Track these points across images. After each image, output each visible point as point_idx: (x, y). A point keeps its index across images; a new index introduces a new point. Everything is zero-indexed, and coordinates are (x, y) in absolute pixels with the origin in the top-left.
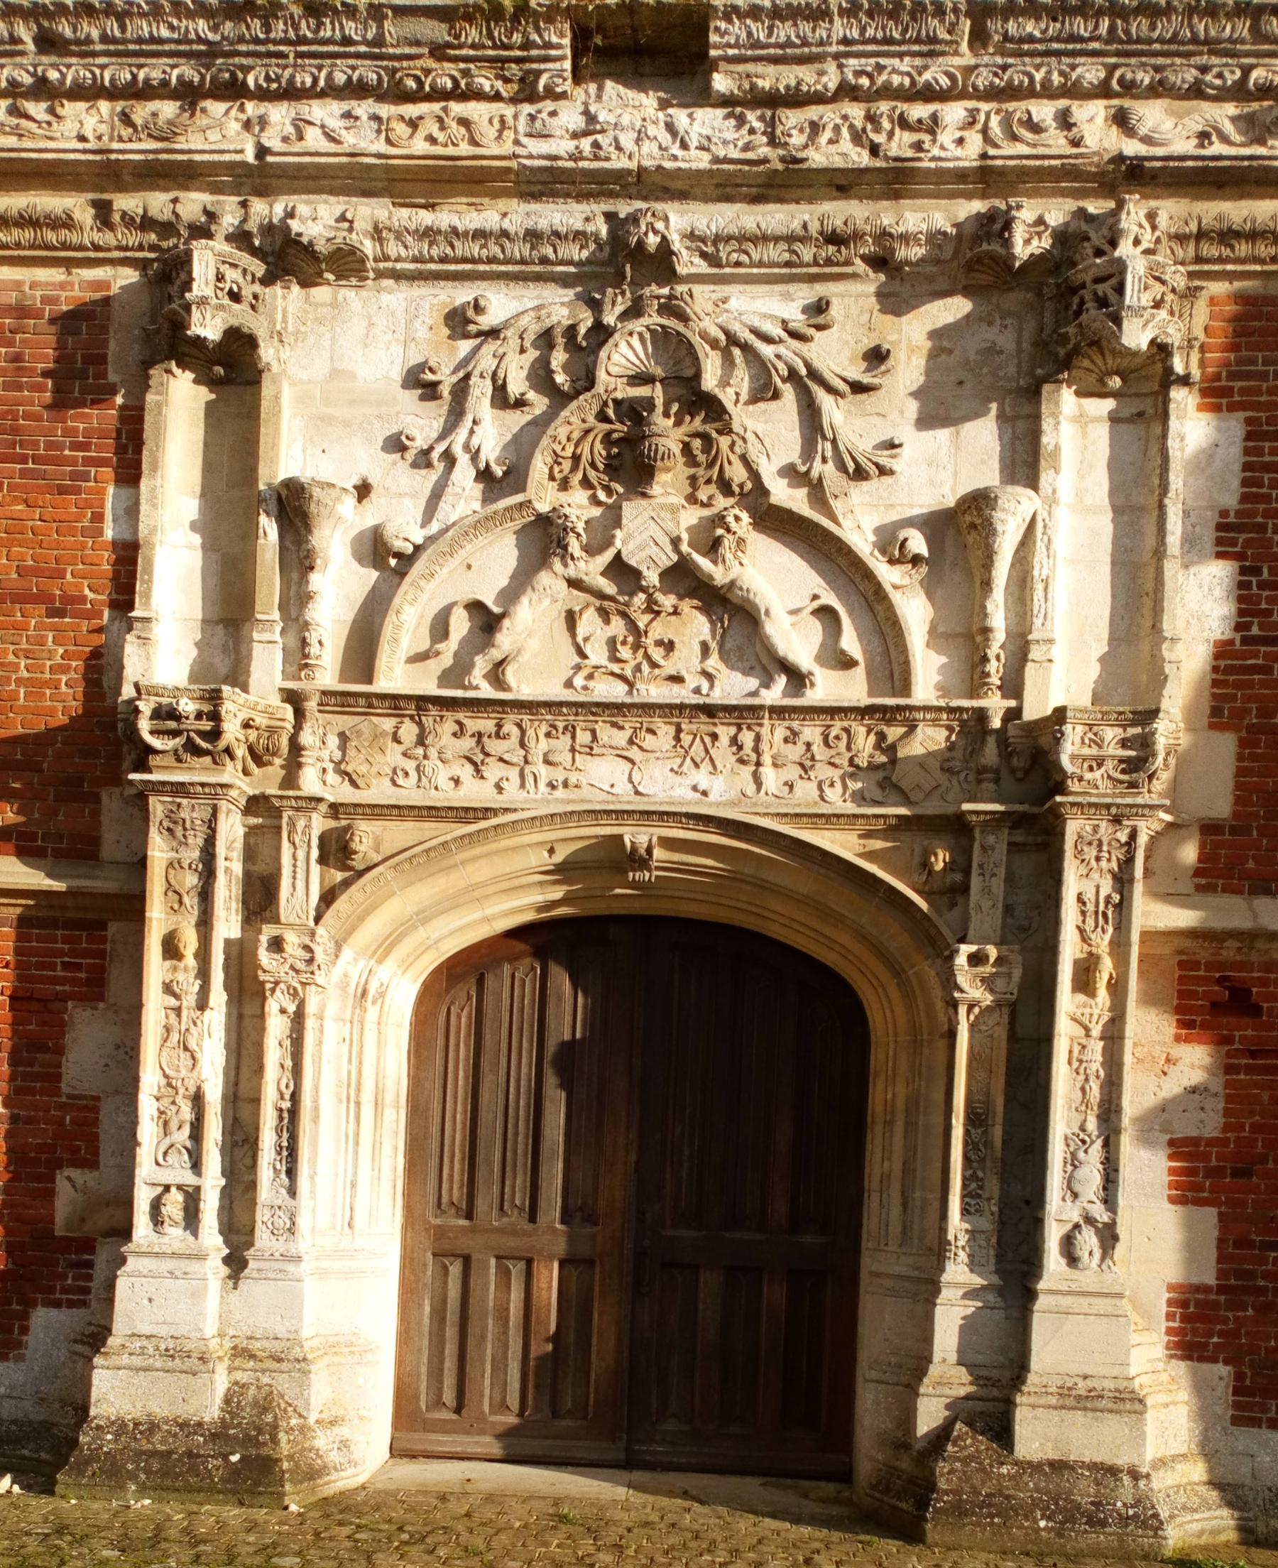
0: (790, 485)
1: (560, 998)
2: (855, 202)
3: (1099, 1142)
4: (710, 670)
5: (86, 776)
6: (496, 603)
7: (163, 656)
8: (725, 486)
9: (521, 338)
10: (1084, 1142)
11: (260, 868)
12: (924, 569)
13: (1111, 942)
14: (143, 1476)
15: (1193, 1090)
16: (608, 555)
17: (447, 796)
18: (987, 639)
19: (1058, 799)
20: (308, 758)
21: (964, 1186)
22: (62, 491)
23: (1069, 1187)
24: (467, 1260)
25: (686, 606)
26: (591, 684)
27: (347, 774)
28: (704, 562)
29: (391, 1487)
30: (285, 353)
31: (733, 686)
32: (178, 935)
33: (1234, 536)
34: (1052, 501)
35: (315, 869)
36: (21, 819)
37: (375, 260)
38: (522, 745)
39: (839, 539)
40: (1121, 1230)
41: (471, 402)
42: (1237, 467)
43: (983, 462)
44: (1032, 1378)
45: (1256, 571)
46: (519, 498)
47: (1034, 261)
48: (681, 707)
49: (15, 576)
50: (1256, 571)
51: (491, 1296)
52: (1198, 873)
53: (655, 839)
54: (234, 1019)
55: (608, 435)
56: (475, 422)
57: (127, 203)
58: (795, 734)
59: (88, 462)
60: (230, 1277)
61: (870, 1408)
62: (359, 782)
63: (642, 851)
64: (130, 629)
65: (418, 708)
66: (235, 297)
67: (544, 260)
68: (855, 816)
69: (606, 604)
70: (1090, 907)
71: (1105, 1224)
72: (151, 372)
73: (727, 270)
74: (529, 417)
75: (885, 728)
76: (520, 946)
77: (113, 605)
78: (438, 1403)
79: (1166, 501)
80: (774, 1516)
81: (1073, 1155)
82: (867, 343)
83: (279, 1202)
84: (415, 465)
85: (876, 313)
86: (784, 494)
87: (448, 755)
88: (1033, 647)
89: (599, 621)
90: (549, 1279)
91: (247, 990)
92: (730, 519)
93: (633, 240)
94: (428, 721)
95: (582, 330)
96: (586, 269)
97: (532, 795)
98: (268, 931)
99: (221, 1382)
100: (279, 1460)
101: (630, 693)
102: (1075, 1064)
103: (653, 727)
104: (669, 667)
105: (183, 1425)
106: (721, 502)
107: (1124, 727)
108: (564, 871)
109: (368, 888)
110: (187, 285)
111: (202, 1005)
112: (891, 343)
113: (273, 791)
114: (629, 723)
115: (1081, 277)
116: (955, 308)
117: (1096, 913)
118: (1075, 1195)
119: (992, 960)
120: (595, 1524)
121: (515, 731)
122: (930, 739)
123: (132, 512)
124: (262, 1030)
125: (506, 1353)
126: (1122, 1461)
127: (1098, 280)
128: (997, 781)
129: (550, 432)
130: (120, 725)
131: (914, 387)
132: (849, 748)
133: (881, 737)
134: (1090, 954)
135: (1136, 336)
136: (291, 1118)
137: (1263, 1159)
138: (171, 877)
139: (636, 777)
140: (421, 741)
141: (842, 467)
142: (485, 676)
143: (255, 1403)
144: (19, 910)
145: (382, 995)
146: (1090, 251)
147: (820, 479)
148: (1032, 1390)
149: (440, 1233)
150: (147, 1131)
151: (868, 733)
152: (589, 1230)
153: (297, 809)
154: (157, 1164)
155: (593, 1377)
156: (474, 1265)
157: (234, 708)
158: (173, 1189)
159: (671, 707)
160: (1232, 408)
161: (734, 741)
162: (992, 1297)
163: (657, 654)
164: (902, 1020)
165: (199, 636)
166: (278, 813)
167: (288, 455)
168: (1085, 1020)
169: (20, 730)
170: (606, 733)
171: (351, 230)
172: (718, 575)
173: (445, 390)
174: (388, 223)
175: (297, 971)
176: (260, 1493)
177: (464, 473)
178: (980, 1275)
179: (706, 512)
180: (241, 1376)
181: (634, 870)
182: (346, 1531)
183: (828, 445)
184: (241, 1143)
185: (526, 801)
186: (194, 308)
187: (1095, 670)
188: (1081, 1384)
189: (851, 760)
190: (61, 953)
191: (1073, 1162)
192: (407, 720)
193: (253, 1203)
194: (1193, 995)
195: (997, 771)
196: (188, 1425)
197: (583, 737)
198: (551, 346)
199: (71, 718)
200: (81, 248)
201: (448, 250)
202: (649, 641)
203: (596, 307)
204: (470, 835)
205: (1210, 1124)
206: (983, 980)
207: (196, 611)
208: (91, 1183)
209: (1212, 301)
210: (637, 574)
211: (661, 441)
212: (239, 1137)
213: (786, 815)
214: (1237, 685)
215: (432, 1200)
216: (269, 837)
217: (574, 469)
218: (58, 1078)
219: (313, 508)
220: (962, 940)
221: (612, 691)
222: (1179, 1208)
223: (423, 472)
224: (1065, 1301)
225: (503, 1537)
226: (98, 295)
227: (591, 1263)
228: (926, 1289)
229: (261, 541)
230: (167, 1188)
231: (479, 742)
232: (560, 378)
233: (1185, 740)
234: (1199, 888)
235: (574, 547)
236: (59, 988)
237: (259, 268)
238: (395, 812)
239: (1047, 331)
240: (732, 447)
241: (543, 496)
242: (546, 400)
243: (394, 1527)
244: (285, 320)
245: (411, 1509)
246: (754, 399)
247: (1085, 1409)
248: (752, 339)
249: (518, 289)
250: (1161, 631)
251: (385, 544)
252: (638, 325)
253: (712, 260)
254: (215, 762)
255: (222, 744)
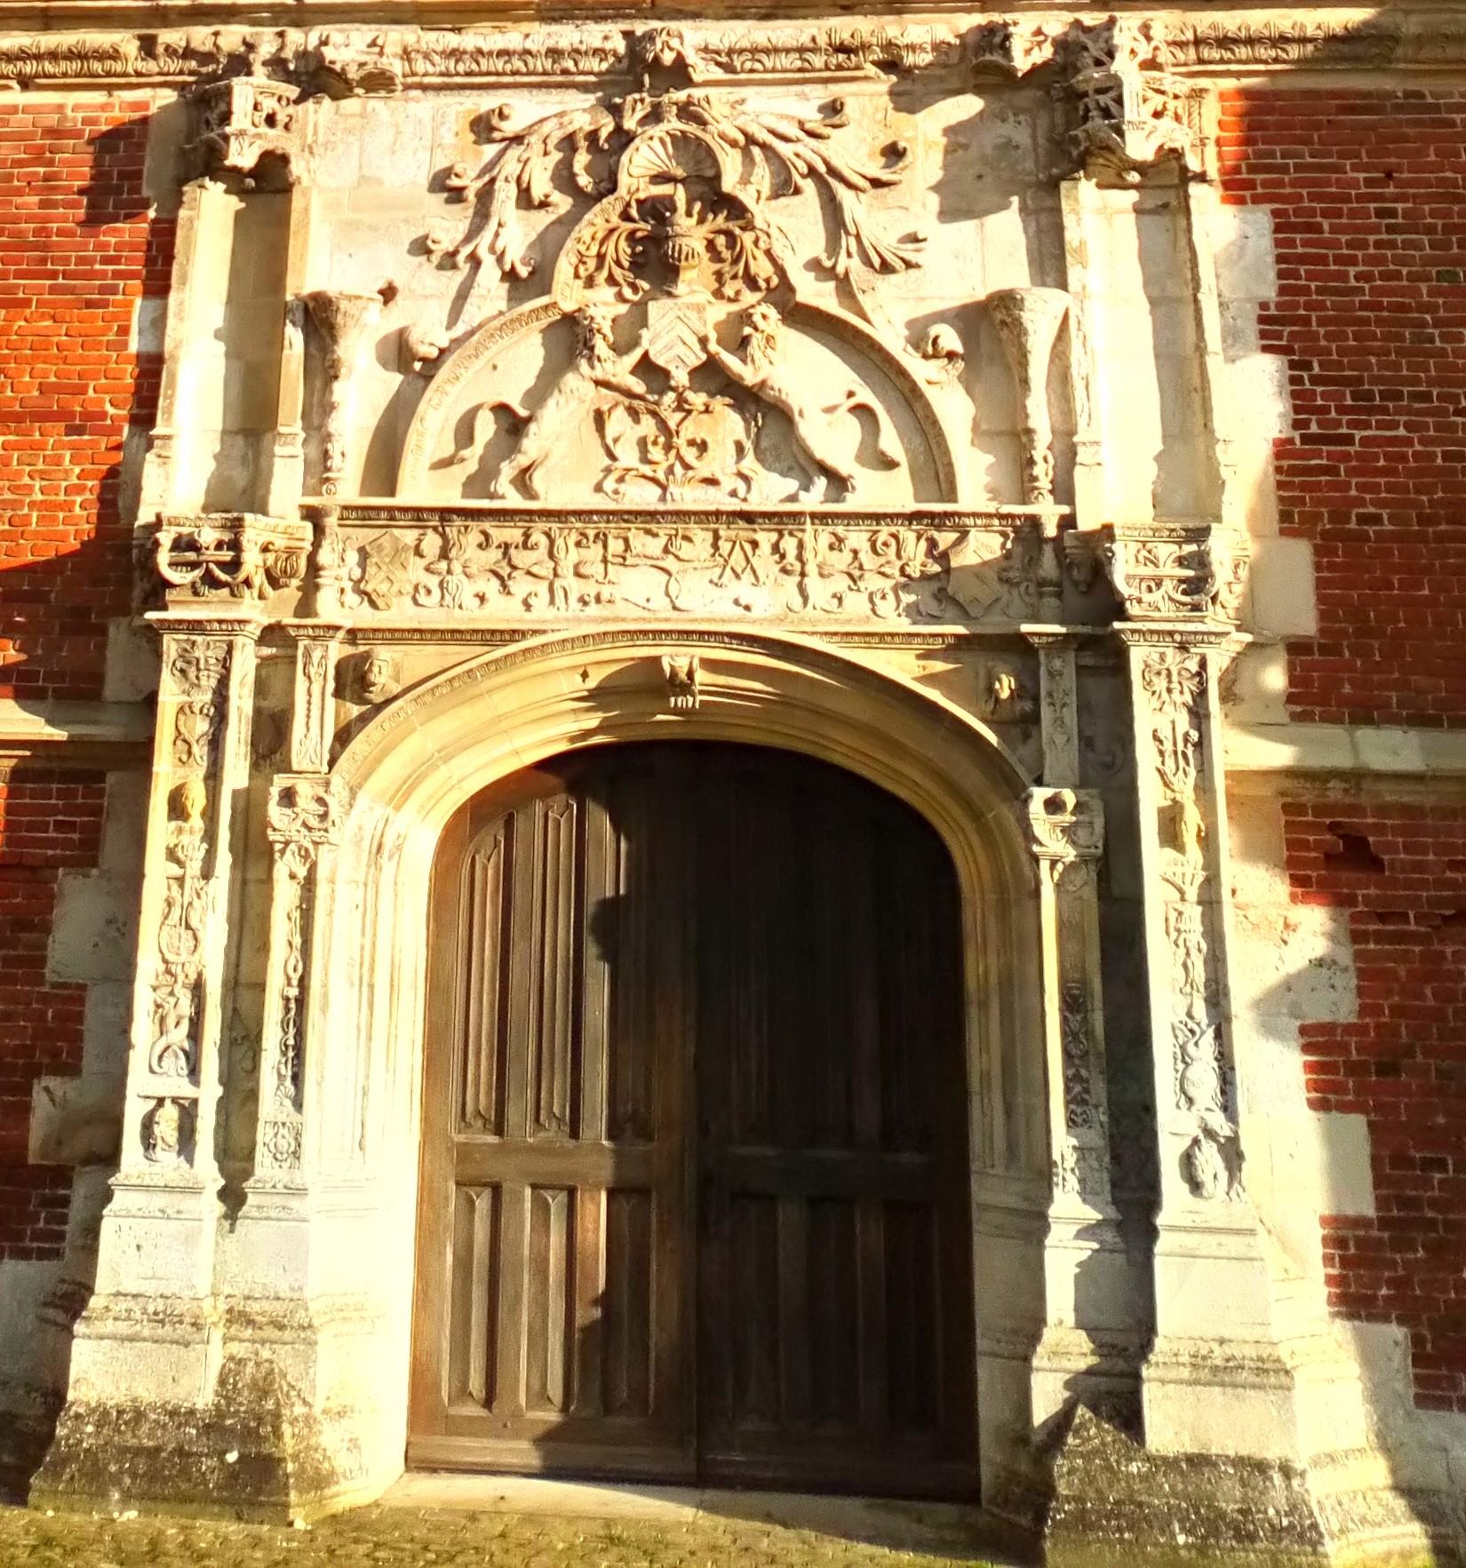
0: (817, 279)
1: (600, 843)
2: (859, 18)
3: (1210, 1033)
4: (746, 472)
5: (92, 607)
6: (523, 404)
7: (175, 488)
8: (752, 283)
9: (545, 142)
10: (1192, 1031)
11: (271, 704)
12: (960, 365)
13: (1196, 788)
14: (128, 1481)
15: (1320, 963)
16: (636, 355)
17: (471, 617)
18: (1032, 440)
19: (1117, 625)
20: (325, 579)
21: (1068, 1090)
22: (90, 304)
23: (1183, 1091)
24: (496, 1190)
25: (719, 403)
26: (622, 488)
27: (366, 594)
28: (731, 361)
29: (408, 1504)
30: (314, 164)
31: (771, 490)
32: (186, 792)
33: (1278, 329)
34: (1082, 297)
35: (331, 702)
36: (23, 657)
37: (404, 76)
38: (551, 555)
39: (868, 337)
40: (1244, 1146)
41: (496, 206)
42: (1270, 259)
43: (1010, 254)
44: (1159, 1343)
45: (1307, 366)
46: (544, 300)
47: (1035, 70)
48: (718, 514)
49: (36, 393)
50: (1307, 366)
51: (527, 1240)
52: (1291, 699)
53: (696, 663)
54: (238, 886)
55: (632, 233)
56: (500, 225)
57: (170, 37)
58: (841, 540)
59: (118, 275)
60: (226, 1217)
61: (990, 1409)
62: (380, 602)
63: (683, 676)
64: (150, 446)
65: (442, 520)
66: (271, 120)
67: (565, 72)
68: (910, 635)
69: (636, 403)
70: (1168, 746)
71: (1227, 1138)
72: (185, 188)
73: (743, 76)
74: (553, 217)
75: (936, 535)
76: (552, 780)
77: (134, 420)
78: (463, 1393)
79: (1200, 296)
80: (870, 1540)
81: (1183, 1048)
82: (884, 140)
83: (281, 1118)
84: (440, 267)
85: (890, 111)
86: (814, 293)
87: (473, 570)
88: (1080, 449)
89: (628, 420)
90: (596, 1213)
91: (254, 851)
92: (757, 318)
93: (650, 57)
94: (451, 532)
95: (604, 134)
96: (607, 78)
97: (563, 613)
98: (280, 781)
99: (215, 1355)
100: (282, 1460)
101: (663, 499)
102: (1174, 935)
103: (689, 534)
104: (703, 469)
105: (173, 1413)
106: (749, 297)
107: (1179, 544)
108: (599, 697)
109: (386, 726)
110: (226, 118)
111: (207, 874)
112: (907, 140)
113: (289, 620)
114: (664, 530)
115: (1082, 87)
116: (968, 106)
117: (1175, 753)
118: (1190, 1101)
119: (1070, 806)
120: (652, 1545)
121: (544, 541)
122: (983, 547)
123: (158, 324)
124: (268, 898)
125: (545, 1322)
126: (1272, 1454)
127: (1100, 91)
128: (1059, 595)
129: (574, 235)
130: (135, 551)
131: (933, 182)
132: (899, 556)
133: (932, 544)
134: (1174, 800)
135: (1140, 147)
136: (298, 1007)
137: (1409, 1052)
138: (181, 723)
139: (673, 591)
140: (444, 554)
141: (868, 262)
142: (512, 482)
143: (254, 1385)
144: (13, 762)
145: (399, 848)
146: (1090, 61)
147: (847, 274)
148: (1161, 1360)
149: (464, 1154)
150: (142, 1030)
151: (919, 538)
152: (641, 1147)
153: (314, 638)
154: (152, 1071)
155: (653, 1355)
156: (505, 1198)
157: (255, 530)
158: (168, 1103)
159: (707, 514)
160: (1257, 200)
161: (776, 548)
162: (1110, 1236)
163: (690, 454)
164: (987, 875)
165: (217, 448)
166: (293, 642)
167: (314, 268)
168: (1179, 882)
169: (30, 558)
170: (639, 541)
171: (381, 54)
172: (750, 376)
173: (470, 194)
174: (416, 46)
175: (310, 829)
176: (261, 1504)
177: (490, 274)
178: (1094, 1206)
179: (734, 308)
180: (237, 1349)
181: (676, 695)
182: (362, 1549)
183: (852, 241)
184: (242, 1039)
185: (556, 620)
186: (232, 139)
187: (1152, 470)
188: (1218, 1351)
189: (902, 570)
190: (55, 810)
191: (1185, 1058)
192: (430, 531)
193: (253, 1119)
194: (1305, 845)
195: (1058, 584)
196: (179, 1414)
197: (616, 546)
198: (574, 149)
199: (83, 543)
200: (125, 75)
201: (474, 67)
202: (680, 442)
203: (616, 111)
204: (496, 661)
205: (1341, 1006)
206: (1063, 830)
207: (217, 422)
208: (71, 1095)
209: (1222, 97)
210: (666, 374)
211: (684, 241)
212: (239, 1033)
213: (835, 634)
214: (1304, 487)
215: (455, 1108)
216: (282, 668)
217: (599, 267)
218: (41, 961)
219: (340, 319)
220: (1039, 782)
221: (642, 496)
222: (1321, 1115)
223: (449, 273)
224: (1191, 1241)
225: (544, 1558)
226: (137, 115)
227: (643, 1192)
228: (1034, 1225)
229: (286, 352)
230: (161, 1102)
231: (505, 554)
232: (584, 180)
233: (1252, 549)
234: (1295, 717)
235: (601, 348)
236: (50, 852)
237: (293, 91)
238: (417, 636)
239: (1060, 129)
240: (756, 243)
241: (567, 293)
242: (570, 200)
243: (418, 1547)
244: (315, 133)
245: (438, 1528)
246: (775, 195)
247: (1222, 1384)
248: (770, 139)
249: (541, 95)
250: (1212, 432)
251: (410, 350)
252: (658, 130)
253: (728, 68)
254: (233, 594)
255: (241, 576)
